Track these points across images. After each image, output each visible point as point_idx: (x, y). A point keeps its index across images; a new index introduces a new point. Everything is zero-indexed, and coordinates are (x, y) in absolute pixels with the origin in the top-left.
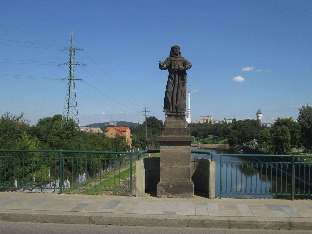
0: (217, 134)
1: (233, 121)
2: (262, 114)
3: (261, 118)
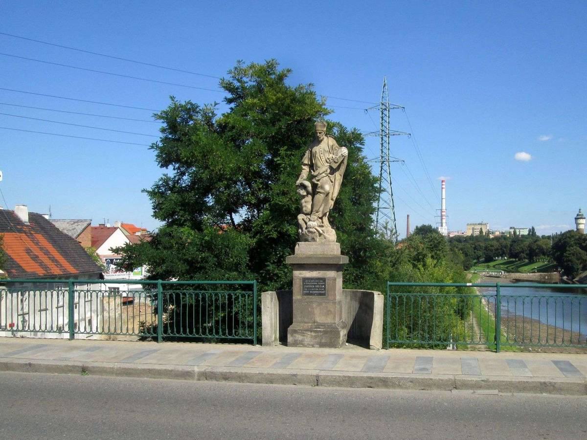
0: (512, 255)
1: (530, 231)
2: (584, 218)
3: (583, 225)
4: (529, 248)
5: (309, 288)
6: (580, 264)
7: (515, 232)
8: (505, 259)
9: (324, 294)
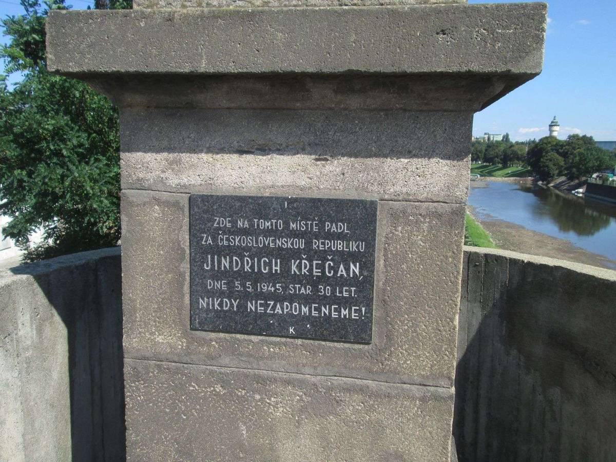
0: (486, 159)
1: (504, 137)
2: (558, 126)
4: (504, 154)
5: (242, 275)
6: (556, 169)
7: (489, 139)
8: (479, 164)
9: (358, 332)
